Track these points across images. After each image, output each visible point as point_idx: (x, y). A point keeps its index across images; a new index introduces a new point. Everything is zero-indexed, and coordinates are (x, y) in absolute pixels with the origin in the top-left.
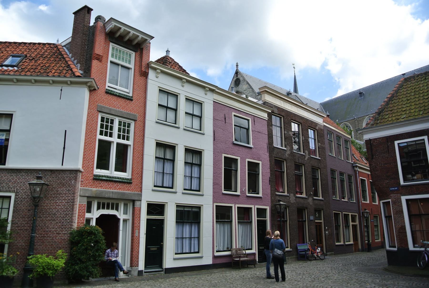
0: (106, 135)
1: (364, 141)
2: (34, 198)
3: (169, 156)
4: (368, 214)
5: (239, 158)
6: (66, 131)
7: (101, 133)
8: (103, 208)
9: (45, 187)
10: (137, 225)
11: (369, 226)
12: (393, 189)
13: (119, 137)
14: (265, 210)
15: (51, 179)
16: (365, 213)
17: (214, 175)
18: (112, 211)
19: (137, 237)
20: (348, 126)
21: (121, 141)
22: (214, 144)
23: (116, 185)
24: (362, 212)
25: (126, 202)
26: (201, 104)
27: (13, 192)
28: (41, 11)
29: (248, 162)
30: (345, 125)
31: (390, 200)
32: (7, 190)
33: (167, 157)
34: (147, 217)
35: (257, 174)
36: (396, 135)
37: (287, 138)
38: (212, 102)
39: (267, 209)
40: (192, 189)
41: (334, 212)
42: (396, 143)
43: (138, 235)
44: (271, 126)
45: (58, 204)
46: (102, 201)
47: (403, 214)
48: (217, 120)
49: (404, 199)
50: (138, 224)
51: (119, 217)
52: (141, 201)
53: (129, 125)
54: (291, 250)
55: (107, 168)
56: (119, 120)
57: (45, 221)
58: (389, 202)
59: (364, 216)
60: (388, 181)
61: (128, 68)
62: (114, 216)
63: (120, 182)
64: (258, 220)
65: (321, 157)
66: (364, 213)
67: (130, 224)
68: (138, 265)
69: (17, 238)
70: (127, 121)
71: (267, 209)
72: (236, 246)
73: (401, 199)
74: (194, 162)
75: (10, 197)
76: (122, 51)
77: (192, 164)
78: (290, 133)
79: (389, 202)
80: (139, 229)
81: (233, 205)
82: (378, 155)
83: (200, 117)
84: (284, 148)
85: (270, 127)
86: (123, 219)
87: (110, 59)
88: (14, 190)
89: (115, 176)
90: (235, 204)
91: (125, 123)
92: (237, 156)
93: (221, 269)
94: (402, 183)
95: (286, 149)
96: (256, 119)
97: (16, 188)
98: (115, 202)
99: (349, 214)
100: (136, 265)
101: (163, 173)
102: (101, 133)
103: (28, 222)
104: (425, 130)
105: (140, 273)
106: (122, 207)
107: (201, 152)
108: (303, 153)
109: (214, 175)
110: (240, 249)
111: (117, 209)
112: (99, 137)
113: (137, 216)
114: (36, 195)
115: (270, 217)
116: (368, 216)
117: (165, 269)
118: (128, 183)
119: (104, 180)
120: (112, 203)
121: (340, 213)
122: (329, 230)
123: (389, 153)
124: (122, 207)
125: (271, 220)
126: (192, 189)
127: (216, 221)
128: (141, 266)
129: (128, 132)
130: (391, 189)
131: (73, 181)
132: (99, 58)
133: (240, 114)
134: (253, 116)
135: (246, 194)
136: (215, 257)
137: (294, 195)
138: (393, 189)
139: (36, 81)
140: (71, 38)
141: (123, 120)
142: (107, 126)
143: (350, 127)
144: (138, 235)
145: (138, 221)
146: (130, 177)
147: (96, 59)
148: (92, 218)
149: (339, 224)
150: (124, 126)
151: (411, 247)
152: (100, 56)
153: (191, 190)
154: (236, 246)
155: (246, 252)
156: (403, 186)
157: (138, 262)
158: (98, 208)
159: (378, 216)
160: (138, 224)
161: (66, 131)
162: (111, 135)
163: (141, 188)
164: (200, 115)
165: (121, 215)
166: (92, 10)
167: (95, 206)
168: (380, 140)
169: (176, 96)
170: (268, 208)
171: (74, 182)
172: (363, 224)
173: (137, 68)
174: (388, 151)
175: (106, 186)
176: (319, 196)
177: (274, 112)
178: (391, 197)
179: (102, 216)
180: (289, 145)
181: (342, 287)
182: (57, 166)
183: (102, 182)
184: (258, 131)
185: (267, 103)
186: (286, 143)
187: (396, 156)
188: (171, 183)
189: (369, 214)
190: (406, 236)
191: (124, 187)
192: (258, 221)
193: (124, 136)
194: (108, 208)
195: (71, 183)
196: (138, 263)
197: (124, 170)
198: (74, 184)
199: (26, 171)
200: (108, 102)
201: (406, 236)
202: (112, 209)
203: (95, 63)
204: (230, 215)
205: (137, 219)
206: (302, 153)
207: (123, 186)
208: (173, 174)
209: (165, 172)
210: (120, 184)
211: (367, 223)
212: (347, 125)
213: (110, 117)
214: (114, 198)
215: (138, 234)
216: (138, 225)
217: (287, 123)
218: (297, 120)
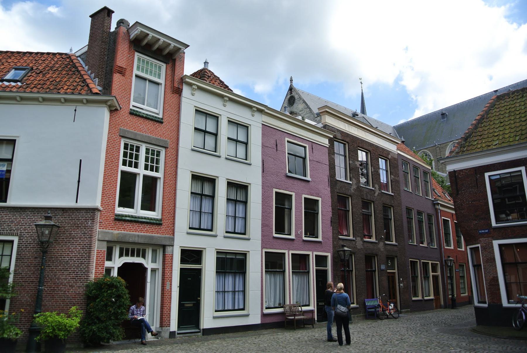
0: (130, 166)
1: (448, 173)
2: (42, 243)
3: (207, 191)
5: (293, 194)
6: (81, 160)
7: (124, 164)
8: (127, 255)
10: (168, 276)
11: (453, 277)
12: (483, 231)
13: (146, 168)
14: (326, 257)
15: (63, 219)
16: (448, 261)
17: (263, 214)
18: (138, 258)
19: (168, 290)
20: (427, 154)
21: (149, 173)
22: (263, 177)
23: (142, 227)
24: (445, 260)
25: (155, 248)
26: (247, 127)
27: (15, 235)
29: (305, 198)
30: (424, 153)
31: (479, 245)
32: (8, 232)
33: (205, 192)
34: (181, 266)
36: (487, 165)
37: (353, 169)
38: (261, 126)
40: (236, 231)
41: (410, 260)
42: (487, 175)
43: (170, 288)
44: (333, 154)
46: (125, 247)
47: (495, 262)
48: (267, 147)
49: (496, 243)
50: (169, 274)
51: (146, 266)
52: (173, 246)
53: (158, 154)
55: (131, 206)
56: (147, 147)
58: (478, 247)
59: (447, 264)
60: (476, 222)
61: (158, 84)
62: (141, 265)
63: (147, 223)
64: (316, 270)
65: (394, 193)
66: (447, 261)
67: (159, 275)
68: (170, 324)
70: (157, 148)
72: (290, 302)
73: (493, 244)
74: (238, 199)
75: (12, 242)
77: (236, 201)
78: (356, 164)
79: (478, 247)
80: (171, 281)
81: (286, 252)
82: (464, 190)
83: (246, 144)
84: (349, 182)
85: (332, 156)
86: (151, 268)
87: (135, 72)
88: (18, 233)
89: (141, 215)
90: (289, 249)
91: (154, 151)
92: (291, 192)
93: (272, 330)
94: (494, 224)
95: (351, 182)
96: (314, 145)
97: (20, 231)
98: (141, 247)
99: (428, 263)
100: (168, 325)
101: (201, 212)
102: (124, 164)
103: (35, 272)
104: (522, 159)
105: (172, 334)
106: (149, 254)
107: (247, 186)
108: (373, 187)
109: (263, 214)
110: (295, 306)
111: (144, 257)
112: (122, 168)
113: (169, 265)
114: (45, 239)
115: (331, 266)
116: (452, 265)
117: (203, 329)
118: (157, 224)
119: (128, 221)
120: (137, 249)
121: (418, 261)
122: (405, 282)
123: (478, 188)
124: (149, 254)
125: (333, 270)
126: (236, 231)
127: (266, 271)
128: (174, 326)
129: (158, 162)
130: (480, 232)
131: (90, 222)
132: (121, 71)
133: (295, 140)
134: (311, 142)
135: (302, 238)
136: (264, 315)
137: (361, 239)
138: (483, 231)
139: (44, 100)
140: (87, 46)
141: (151, 147)
142: (131, 155)
143: (430, 156)
144: (170, 288)
145: (170, 270)
146: (159, 217)
147: (118, 72)
148: (114, 267)
149: (417, 275)
150: (153, 154)
151: (505, 303)
152: (123, 68)
153: (234, 233)
154: (290, 302)
155: (302, 309)
156: (496, 228)
157: (170, 321)
158: (121, 255)
159: (464, 264)
160: (169, 274)
161: (81, 160)
162: (136, 166)
163: (174, 230)
164: (245, 141)
165: (148, 263)
166: (113, 12)
167: (116, 252)
168: (467, 172)
169: (216, 118)
170: (329, 255)
171: (91, 223)
172: (446, 274)
173: (169, 83)
174: (477, 185)
175: (131, 228)
176: (391, 240)
177: (337, 137)
178: (480, 241)
179: (125, 264)
180: (355, 178)
182: (70, 203)
183: (125, 223)
184: (317, 161)
185: (328, 126)
186: (351, 176)
187: (486, 192)
188: (210, 224)
189: (453, 262)
190: (499, 289)
191: (153, 230)
193: (152, 167)
194: (133, 255)
195: (88, 225)
196: (170, 323)
197: (153, 209)
198: (91, 225)
199: (31, 210)
201: (499, 289)
202: (138, 256)
203: (117, 77)
204: (282, 264)
205: (168, 269)
206: (371, 188)
207: (152, 228)
208: (212, 214)
209: (203, 210)
210: (148, 226)
211: (450, 273)
212: (426, 154)
213: (136, 143)
214: (140, 242)
215: (170, 286)
216: (169, 276)
217: (352, 151)
218: (365, 147)
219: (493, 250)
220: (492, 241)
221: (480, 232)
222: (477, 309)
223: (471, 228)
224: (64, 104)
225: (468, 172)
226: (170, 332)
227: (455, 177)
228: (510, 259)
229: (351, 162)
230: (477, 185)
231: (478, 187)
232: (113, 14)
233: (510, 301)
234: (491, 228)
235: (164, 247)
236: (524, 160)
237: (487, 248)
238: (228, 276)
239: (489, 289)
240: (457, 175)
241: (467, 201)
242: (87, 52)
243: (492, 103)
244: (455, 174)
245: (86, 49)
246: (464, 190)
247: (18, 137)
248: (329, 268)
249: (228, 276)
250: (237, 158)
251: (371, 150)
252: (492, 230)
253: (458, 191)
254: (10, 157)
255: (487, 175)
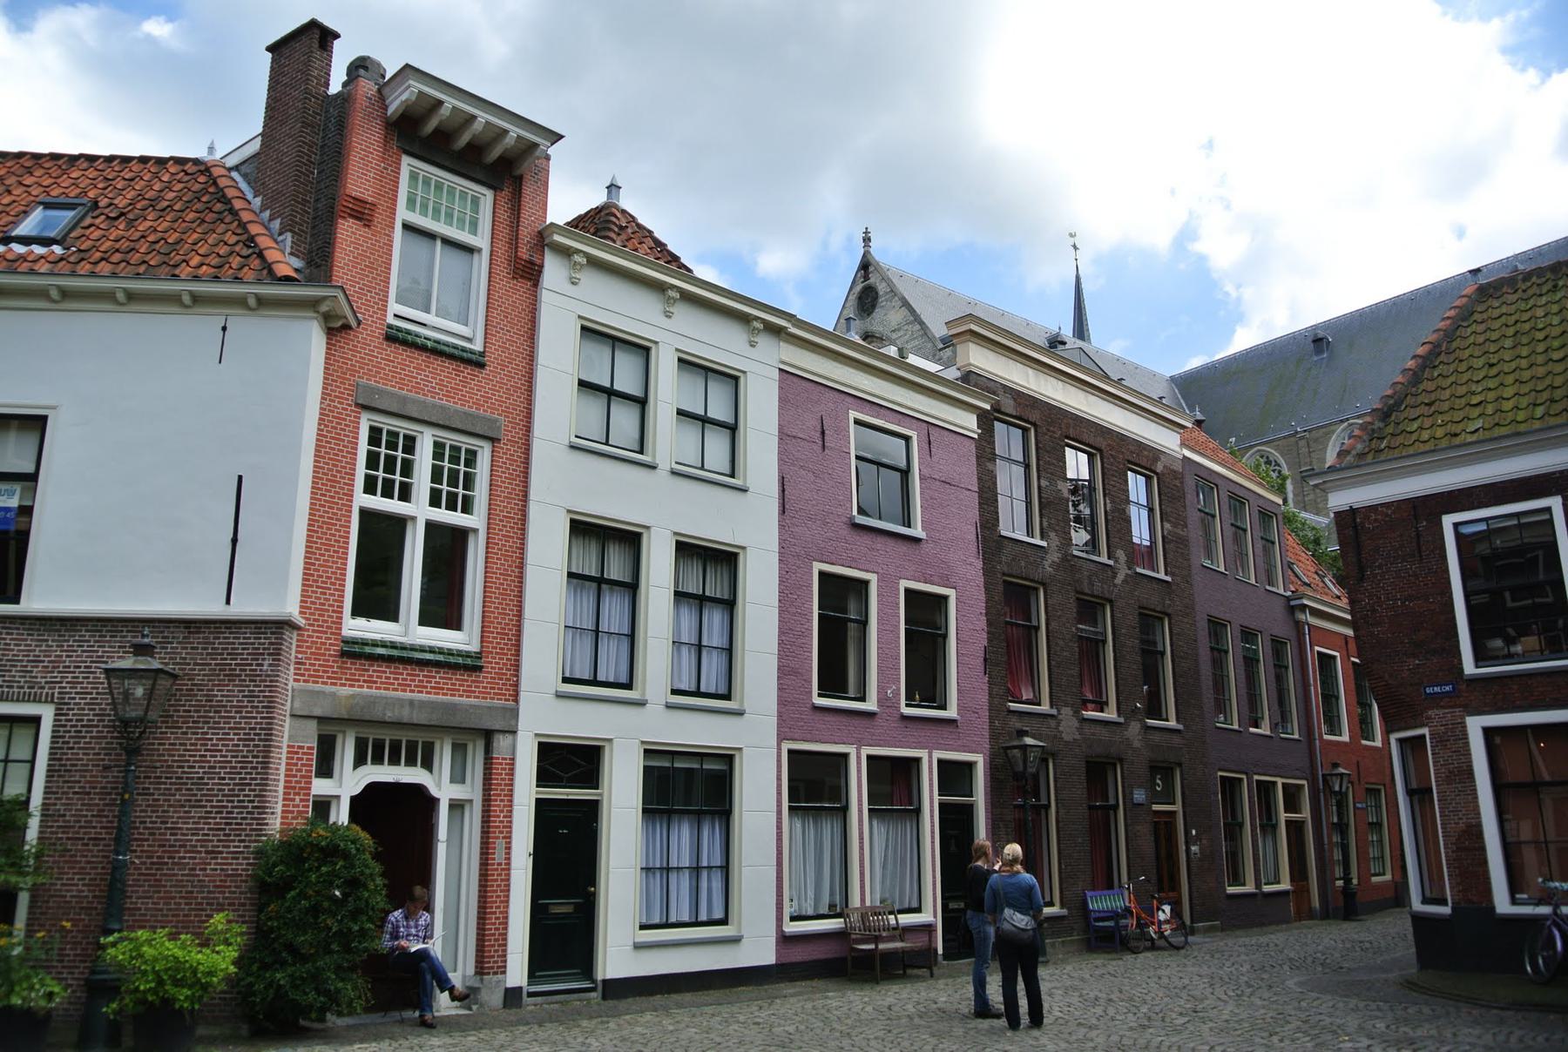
0: (388, 493)
2: (126, 723)
3: (616, 569)
4: (1345, 780)
5: (873, 578)
6: (240, 478)
7: (370, 488)
8: (378, 760)
9: (163, 683)
10: (500, 822)
11: (1347, 825)
12: (1437, 689)
13: (435, 501)
14: (970, 766)
15: (186, 654)
16: (1334, 778)
17: (784, 638)
18: (411, 770)
19: (500, 864)
21: (443, 515)
22: (782, 526)
23: (423, 676)
24: (1323, 775)
25: (461, 738)
26: (736, 379)
27: (46, 702)
28: (150, 39)
31: (1425, 731)
32: (25, 693)
33: (609, 574)
34: (537, 793)
35: (940, 635)
36: (1448, 492)
37: (1049, 503)
38: (776, 374)
39: (976, 763)
40: (703, 689)
41: (1220, 773)
42: (1448, 521)
43: (506, 859)
45: (212, 745)
46: (372, 735)
47: (1474, 781)
48: (794, 437)
49: (1475, 726)
50: (504, 817)
51: (434, 792)
52: (514, 733)
53: (471, 458)
54: (1065, 912)
55: (390, 613)
56: (437, 439)
57: (163, 806)
58: (1423, 736)
59: (1330, 788)
60: (1417, 662)
61: (469, 250)
62: (418, 790)
63: (438, 664)
64: (941, 805)
66: (1329, 778)
67: (474, 818)
68: (505, 967)
69: (64, 868)
70: (466, 442)
71: (976, 763)
73: (1466, 727)
74: (707, 594)
76: (446, 186)
77: (701, 600)
78: (1059, 487)
79: (1423, 736)
80: (509, 838)
82: (1380, 567)
83: (732, 429)
84: (1037, 541)
85: (988, 464)
86: (450, 800)
87: (403, 214)
88: (53, 694)
89: (419, 642)
90: (860, 743)
91: (458, 449)
92: (867, 571)
93: (808, 983)
94: (1469, 667)
95: (1044, 544)
96: (934, 433)
98: (421, 738)
99: (1274, 783)
100: (498, 967)
101: (597, 631)
102: (370, 488)
103: (104, 811)
104: (1554, 473)
105: (513, 997)
106: (444, 757)
107: (735, 555)
108: (1109, 558)
109: (784, 638)
110: (877, 910)
111: (428, 765)
112: (363, 500)
113: (501, 790)
114: (133, 713)
115: (986, 794)
116: (1344, 789)
117: (604, 981)
118: (466, 668)
119: (381, 658)
120: (408, 741)
121: (1244, 777)
122: (1204, 842)
123: (1421, 560)
124: (444, 757)
125: (992, 804)
126: (703, 689)
128: (517, 972)
129: (469, 482)
130: (1428, 690)
131: (266, 662)
132: (360, 212)
133: (877, 417)
134: (925, 424)
135: (898, 708)
136: (785, 940)
137: (1075, 712)
138: (1437, 689)
139: (132, 297)
140: (260, 138)
141: (450, 438)
142: (390, 461)
144: (506, 859)
145: (504, 806)
146: (474, 647)
147: (351, 216)
148: (338, 797)
149: (1240, 820)
150: (455, 459)
151: (1502, 903)
152: (367, 203)
153: (697, 693)
155: (900, 922)
156: (1475, 680)
157: (505, 956)
158: (360, 761)
160: (504, 817)
161: (240, 478)
162: (405, 495)
163: (516, 685)
164: (730, 420)
165: (441, 785)
166: (337, 36)
167: (346, 751)
168: (1389, 512)
169: (643, 350)
170: (979, 760)
171: (270, 665)
172: (1328, 818)
174: (1420, 552)
175: (389, 678)
176: (1164, 717)
177: (1003, 409)
178: (1429, 718)
179: (373, 788)
180: (1056, 531)
181: (1250, 1049)
182: (208, 605)
183: (373, 666)
184: (943, 479)
185: (975, 376)
186: (1045, 524)
187: (1447, 571)
188: (624, 667)
189: (1349, 782)
190: (1484, 862)
191: (454, 684)
192: (943, 807)
193: (452, 498)
194: (395, 761)
195: (261, 670)
196: (506, 961)
197: (454, 622)
198: (272, 671)
199: (93, 626)
200: (394, 372)
201: (1484, 862)
202: (411, 762)
204: (840, 787)
205: (501, 801)
206: (1104, 559)
207: (451, 679)
208: (632, 637)
209: (604, 627)
210: (439, 673)
211: (1340, 815)
213: (403, 427)
215: (506, 854)
216: (503, 822)
217: (1048, 449)
219: (1467, 744)
220: (1463, 718)
221: (1428, 691)
222: (1419, 920)
223: (1402, 678)
224: (190, 311)
225: (1394, 512)
226: (507, 990)
227: (1355, 527)
228: (1516, 772)
229: (1044, 483)
230: (1420, 552)
231: (1421, 556)
232: (336, 42)
233: (1518, 896)
234: (1462, 678)
235: (488, 736)
236: (1558, 478)
237: (1449, 740)
238: (679, 822)
239: (1454, 860)
240: (1358, 520)
241: (1389, 600)
242: (258, 154)
243: (1463, 306)
244: (1355, 520)
245: (256, 146)
246: (1380, 567)
247: (54, 408)
248: (980, 798)
249: (679, 822)
250: (706, 470)
251: (1103, 448)
252: (1464, 686)
253: (1362, 569)
254: (30, 469)
255: (1448, 521)
